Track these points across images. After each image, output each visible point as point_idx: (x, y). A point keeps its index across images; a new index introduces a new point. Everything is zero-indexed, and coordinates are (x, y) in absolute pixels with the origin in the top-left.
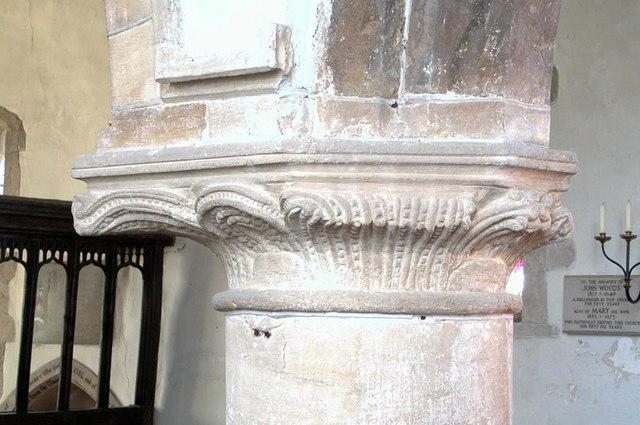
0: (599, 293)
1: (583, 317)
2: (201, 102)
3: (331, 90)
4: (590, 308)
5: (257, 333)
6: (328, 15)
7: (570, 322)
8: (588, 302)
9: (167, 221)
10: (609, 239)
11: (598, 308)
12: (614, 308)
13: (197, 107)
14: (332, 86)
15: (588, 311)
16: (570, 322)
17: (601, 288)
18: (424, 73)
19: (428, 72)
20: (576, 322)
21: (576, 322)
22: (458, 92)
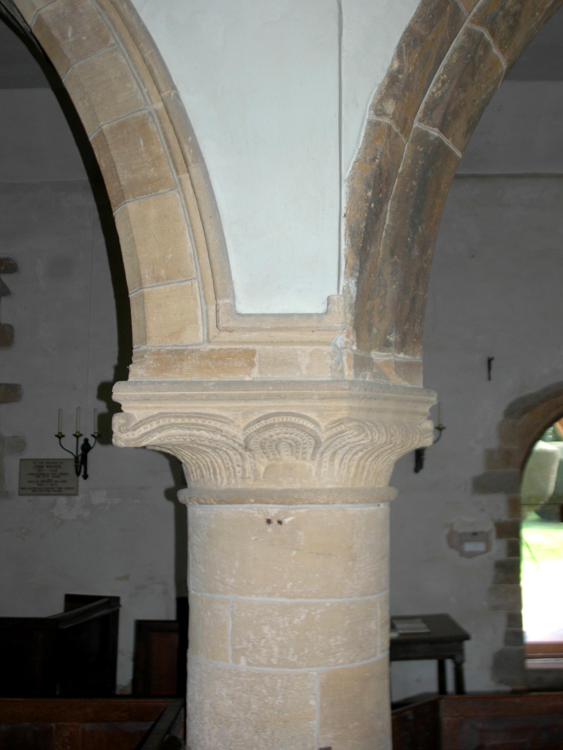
0: (46, 470)
1: (35, 485)
2: (251, 347)
3: (355, 348)
4: (39, 480)
5: (269, 521)
6: (355, 298)
7: (23, 488)
8: (38, 476)
9: (218, 437)
10: (63, 436)
11: (45, 479)
12: (57, 479)
13: (246, 351)
14: (355, 343)
15: (37, 481)
16: (23, 488)
17: (47, 467)
18: (388, 340)
19: (391, 339)
20: (29, 489)
21: (29, 489)
22: (405, 354)
